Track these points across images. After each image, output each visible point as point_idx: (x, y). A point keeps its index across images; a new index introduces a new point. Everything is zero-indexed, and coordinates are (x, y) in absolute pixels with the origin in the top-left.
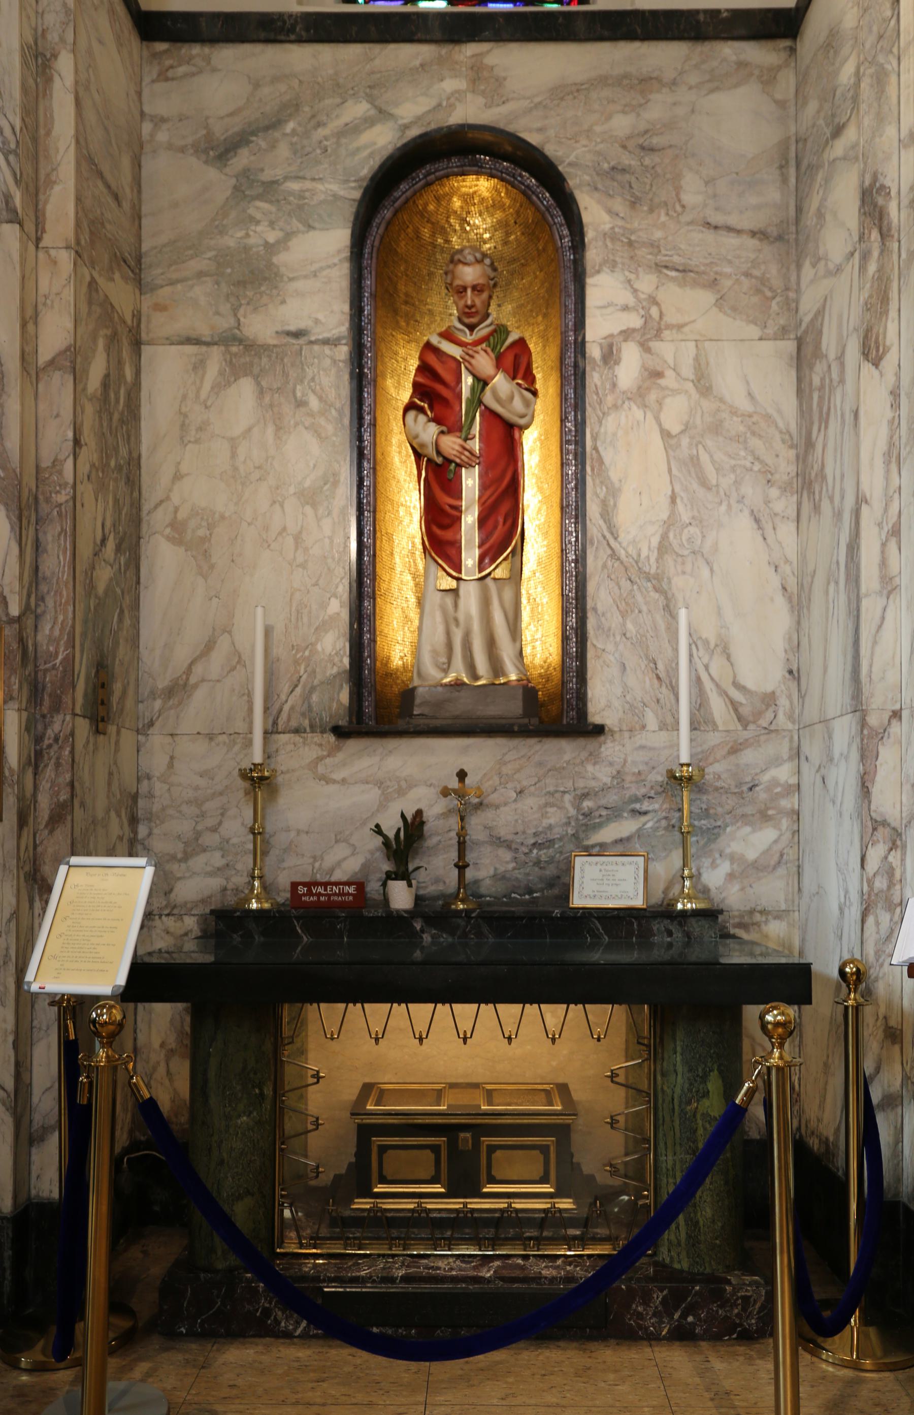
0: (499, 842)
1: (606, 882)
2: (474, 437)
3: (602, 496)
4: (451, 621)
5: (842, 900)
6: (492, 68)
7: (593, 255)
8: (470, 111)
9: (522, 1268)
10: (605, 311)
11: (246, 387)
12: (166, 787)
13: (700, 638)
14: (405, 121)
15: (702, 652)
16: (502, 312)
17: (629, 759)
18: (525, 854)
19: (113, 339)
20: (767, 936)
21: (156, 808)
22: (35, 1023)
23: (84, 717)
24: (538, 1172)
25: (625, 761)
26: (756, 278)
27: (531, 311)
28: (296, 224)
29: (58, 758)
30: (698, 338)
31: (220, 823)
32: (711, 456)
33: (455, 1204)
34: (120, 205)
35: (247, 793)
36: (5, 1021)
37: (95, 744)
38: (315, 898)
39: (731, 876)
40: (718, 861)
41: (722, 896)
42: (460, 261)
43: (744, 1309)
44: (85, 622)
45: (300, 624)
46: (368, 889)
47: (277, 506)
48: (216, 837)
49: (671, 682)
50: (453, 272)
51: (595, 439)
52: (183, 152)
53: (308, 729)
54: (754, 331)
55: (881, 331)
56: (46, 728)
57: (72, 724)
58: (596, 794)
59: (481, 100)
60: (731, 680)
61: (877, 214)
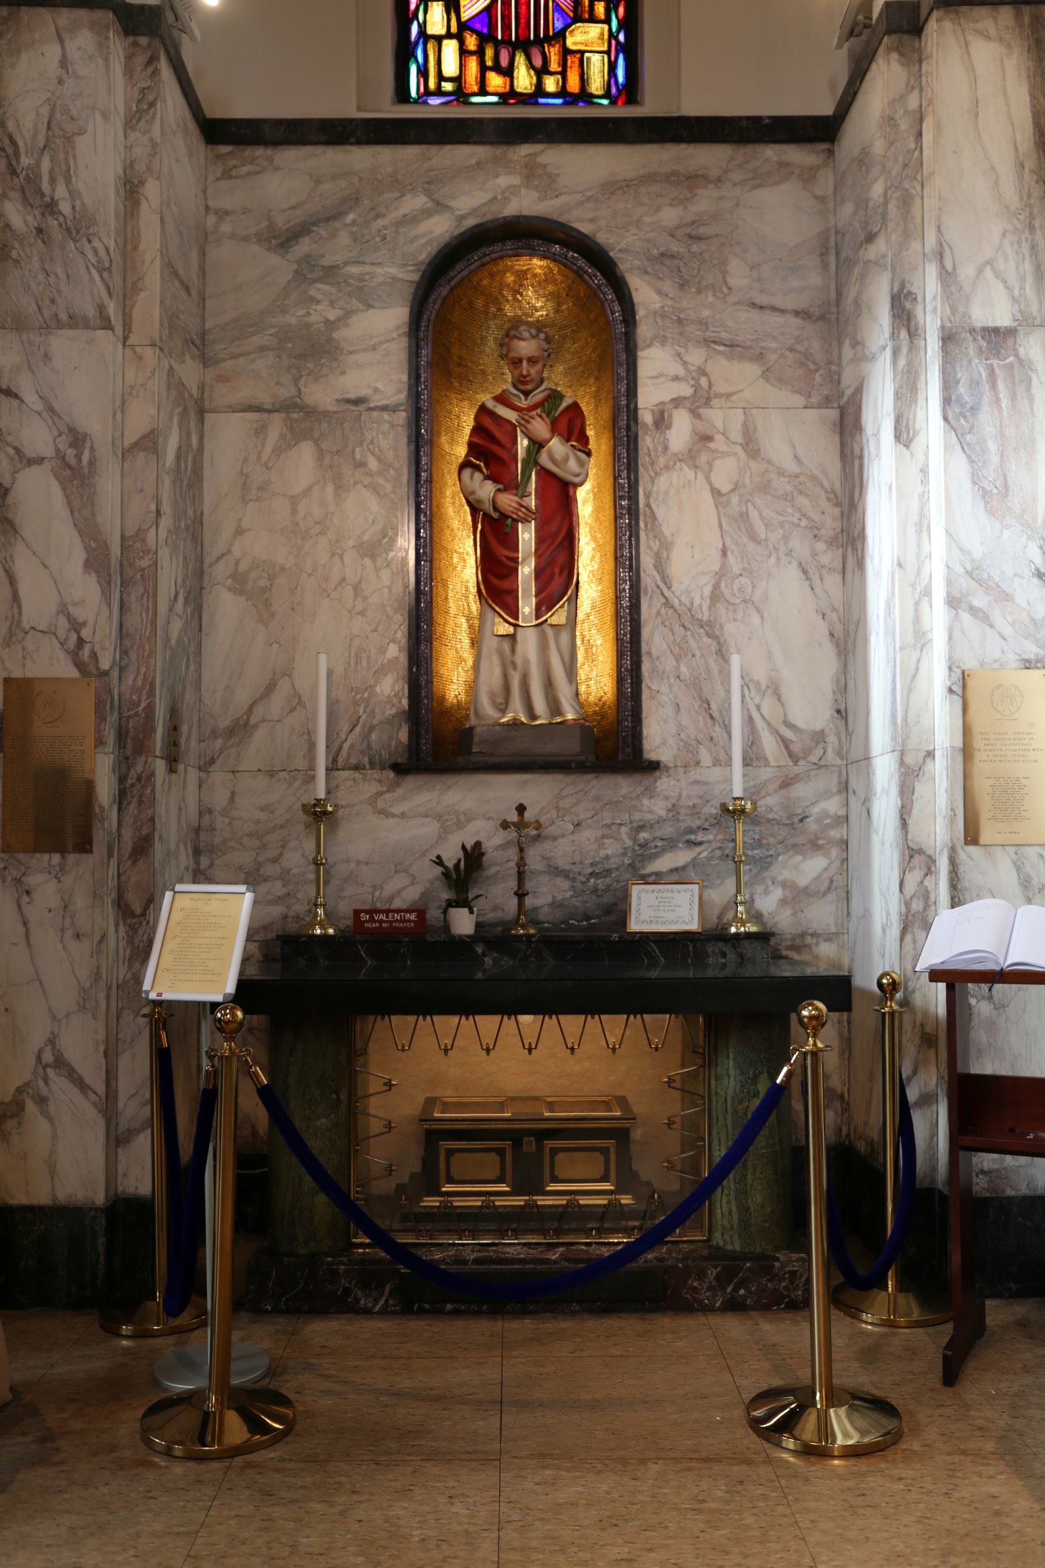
0: (556, 871)
1: (662, 908)
2: (530, 494)
3: (655, 549)
4: (508, 665)
5: (885, 921)
6: (545, 166)
7: (644, 330)
8: (525, 204)
9: (587, 1251)
10: (656, 381)
11: (306, 450)
12: (227, 820)
13: (752, 680)
14: (462, 212)
15: (753, 694)
16: (557, 378)
17: (684, 794)
18: (583, 883)
19: (185, 412)
20: (817, 957)
21: (217, 840)
22: (120, 1036)
23: (162, 758)
24: (599, 1172)
25: (680, 795)
26: (800, 352)
27: (583, 372)
28: (355, 303)
29: (141, 796)
30: (746, 405)
31: (281, 855)
32: (760, 513)
33: (519, 1201)
34: (189, 295)
35: (307, 826)
36: (96, 1032)
38: (377, 925)
39: (783, 902)
40: (771, 888)
41: (776, 919)
42: (515, 337)
43: (791, 1282)
44: (163, 672)
45: (359, 667)
46: (428, 916)
47: (337, 559)
48: (277, 867)
49: (724, 721)
50: (508, 346)
51: (648, 496)
52: (246, 241)
53: (368, 767)
54: (799, 400)
55: (911, 417)
56: (129, 769)
58: (652, 826)
59: (534, 195)
60: (782, 719)
61: (905, 317)
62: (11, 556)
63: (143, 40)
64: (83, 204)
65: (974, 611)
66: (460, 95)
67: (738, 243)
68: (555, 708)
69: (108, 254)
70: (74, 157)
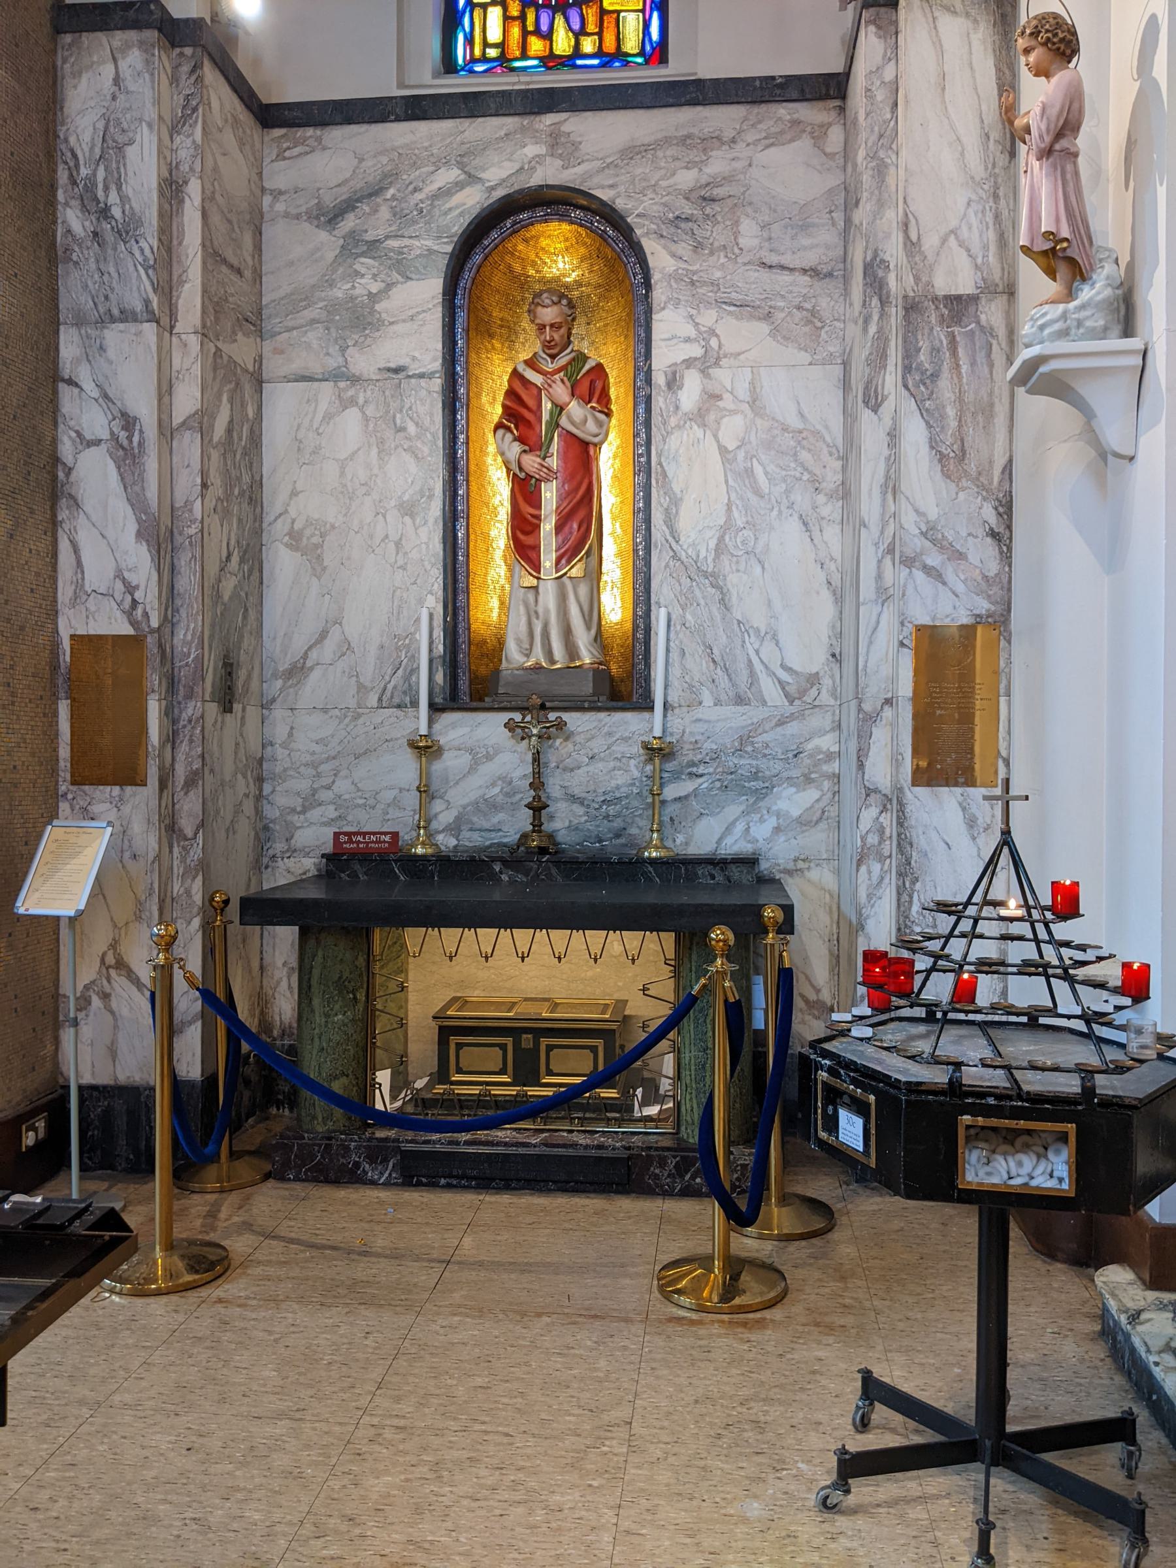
0: (573, 799)
3: (665, 505)
4: (532, 614)
7: (659, 294)
8: (551, 173)
10: (669, 343)
15: (753, 639)
17: (687, 731)
25: (684, 732)
26: (807, 310)
31: (334, 782)
37: (223, 722)
39: (777, 830)
40: (766, 817)
42: (538, 304)
44: (213, 626)
50: (535, 314)
51: (659, 455)
54: (805, 357)
56: (181, 713)
57: (199, 708)
59: (559, 163)
62: (75, 527)
63: (188, 51)
64: (131, 208)
65: (928, 570)
66: (503, 59)
67: (750, 204)
68: (572, 651)
69: (153, 252)
70: (124, 165)
